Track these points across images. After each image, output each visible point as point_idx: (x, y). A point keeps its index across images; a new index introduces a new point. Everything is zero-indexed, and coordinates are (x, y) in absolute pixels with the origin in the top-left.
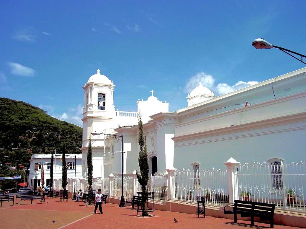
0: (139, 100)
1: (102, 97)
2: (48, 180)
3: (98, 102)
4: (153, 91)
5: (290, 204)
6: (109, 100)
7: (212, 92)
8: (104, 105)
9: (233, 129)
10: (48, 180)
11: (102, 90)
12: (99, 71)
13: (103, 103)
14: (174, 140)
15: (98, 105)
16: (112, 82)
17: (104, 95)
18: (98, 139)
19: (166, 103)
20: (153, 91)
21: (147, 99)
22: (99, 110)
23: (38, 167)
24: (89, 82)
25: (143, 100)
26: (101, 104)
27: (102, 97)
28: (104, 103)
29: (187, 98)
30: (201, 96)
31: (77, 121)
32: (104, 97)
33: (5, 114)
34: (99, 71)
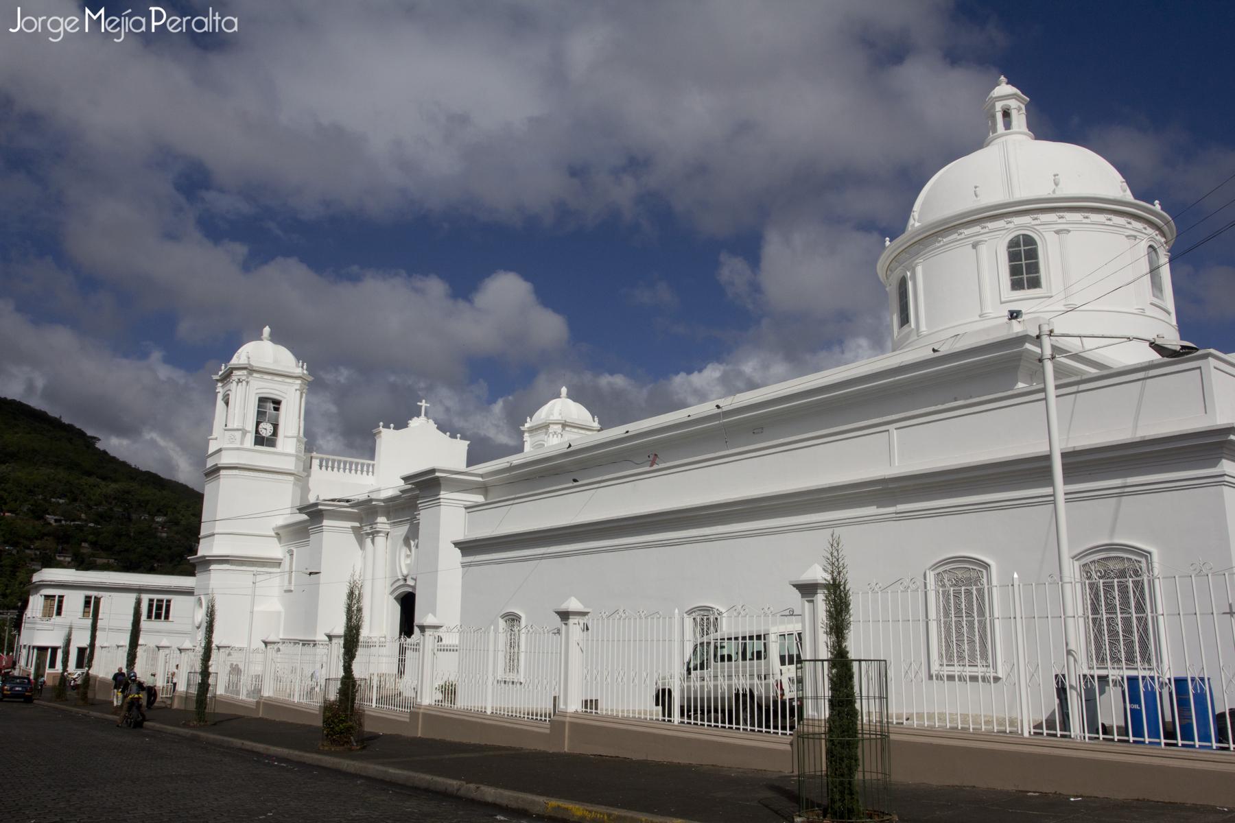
0: (381, 424)
1: (269, 407)
2: (81, 651)
3: (258, 424)
4: (424, 401)
5: (1024, 265)
6: (291, 421)
7: (593, 418)
8: (275, 433)
9: (299, 427)
10: (81, 651)
11: (271, 388)
12: (267, 330)
13: (272, 428)
14: (459, 548)
15: (257, 432)
16: (305, 367)
17: (277, 403)
18: (538, 561)
19: (461, 438)
20: (424, 401)
21: (405, 425)
22: (259, 448)
23: (55, 606)
24: (235, 361)
25: (392, 425)
26: (266, 429)
27: (269, 407)
28: (276, 426)
29: (522, 428)
30: (564, 425)
31: (184, 472)
32: (277, 409)
33: (836, 590)
34: (267, 330)
